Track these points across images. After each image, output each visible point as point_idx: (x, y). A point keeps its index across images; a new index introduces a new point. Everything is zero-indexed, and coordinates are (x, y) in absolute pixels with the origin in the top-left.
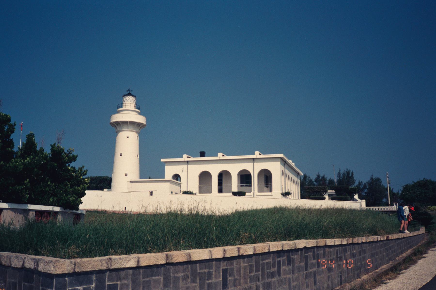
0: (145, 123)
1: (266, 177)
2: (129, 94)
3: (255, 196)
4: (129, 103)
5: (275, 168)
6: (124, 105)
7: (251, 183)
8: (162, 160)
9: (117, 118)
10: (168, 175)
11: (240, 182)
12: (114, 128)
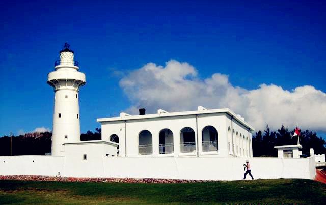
0: (84, 80)
1: (211, 133)
2: (66, 50)
3: (199, 155)
4: (67, 58)
5: (221, 124)
6: (61, 61)
7: (194, 141)
8: (98, 120)
9: (54, 76)
10: (106, 136)
11: (183, 140)
12: (52, 87)
